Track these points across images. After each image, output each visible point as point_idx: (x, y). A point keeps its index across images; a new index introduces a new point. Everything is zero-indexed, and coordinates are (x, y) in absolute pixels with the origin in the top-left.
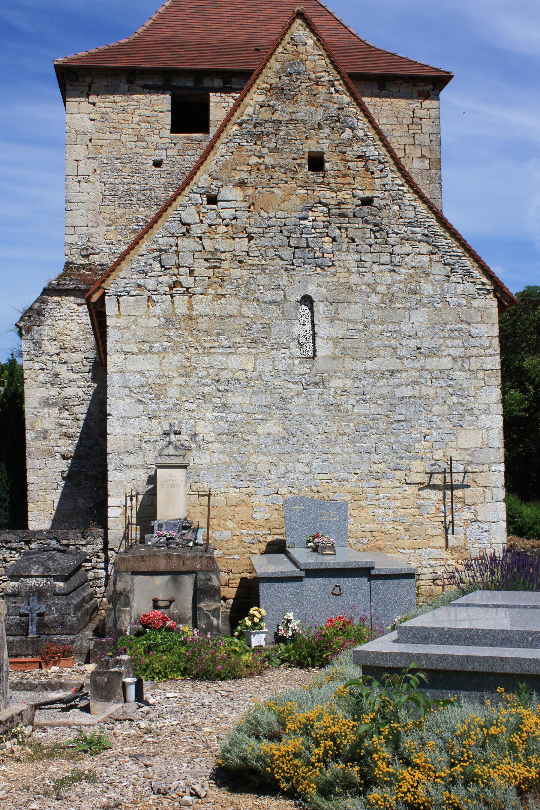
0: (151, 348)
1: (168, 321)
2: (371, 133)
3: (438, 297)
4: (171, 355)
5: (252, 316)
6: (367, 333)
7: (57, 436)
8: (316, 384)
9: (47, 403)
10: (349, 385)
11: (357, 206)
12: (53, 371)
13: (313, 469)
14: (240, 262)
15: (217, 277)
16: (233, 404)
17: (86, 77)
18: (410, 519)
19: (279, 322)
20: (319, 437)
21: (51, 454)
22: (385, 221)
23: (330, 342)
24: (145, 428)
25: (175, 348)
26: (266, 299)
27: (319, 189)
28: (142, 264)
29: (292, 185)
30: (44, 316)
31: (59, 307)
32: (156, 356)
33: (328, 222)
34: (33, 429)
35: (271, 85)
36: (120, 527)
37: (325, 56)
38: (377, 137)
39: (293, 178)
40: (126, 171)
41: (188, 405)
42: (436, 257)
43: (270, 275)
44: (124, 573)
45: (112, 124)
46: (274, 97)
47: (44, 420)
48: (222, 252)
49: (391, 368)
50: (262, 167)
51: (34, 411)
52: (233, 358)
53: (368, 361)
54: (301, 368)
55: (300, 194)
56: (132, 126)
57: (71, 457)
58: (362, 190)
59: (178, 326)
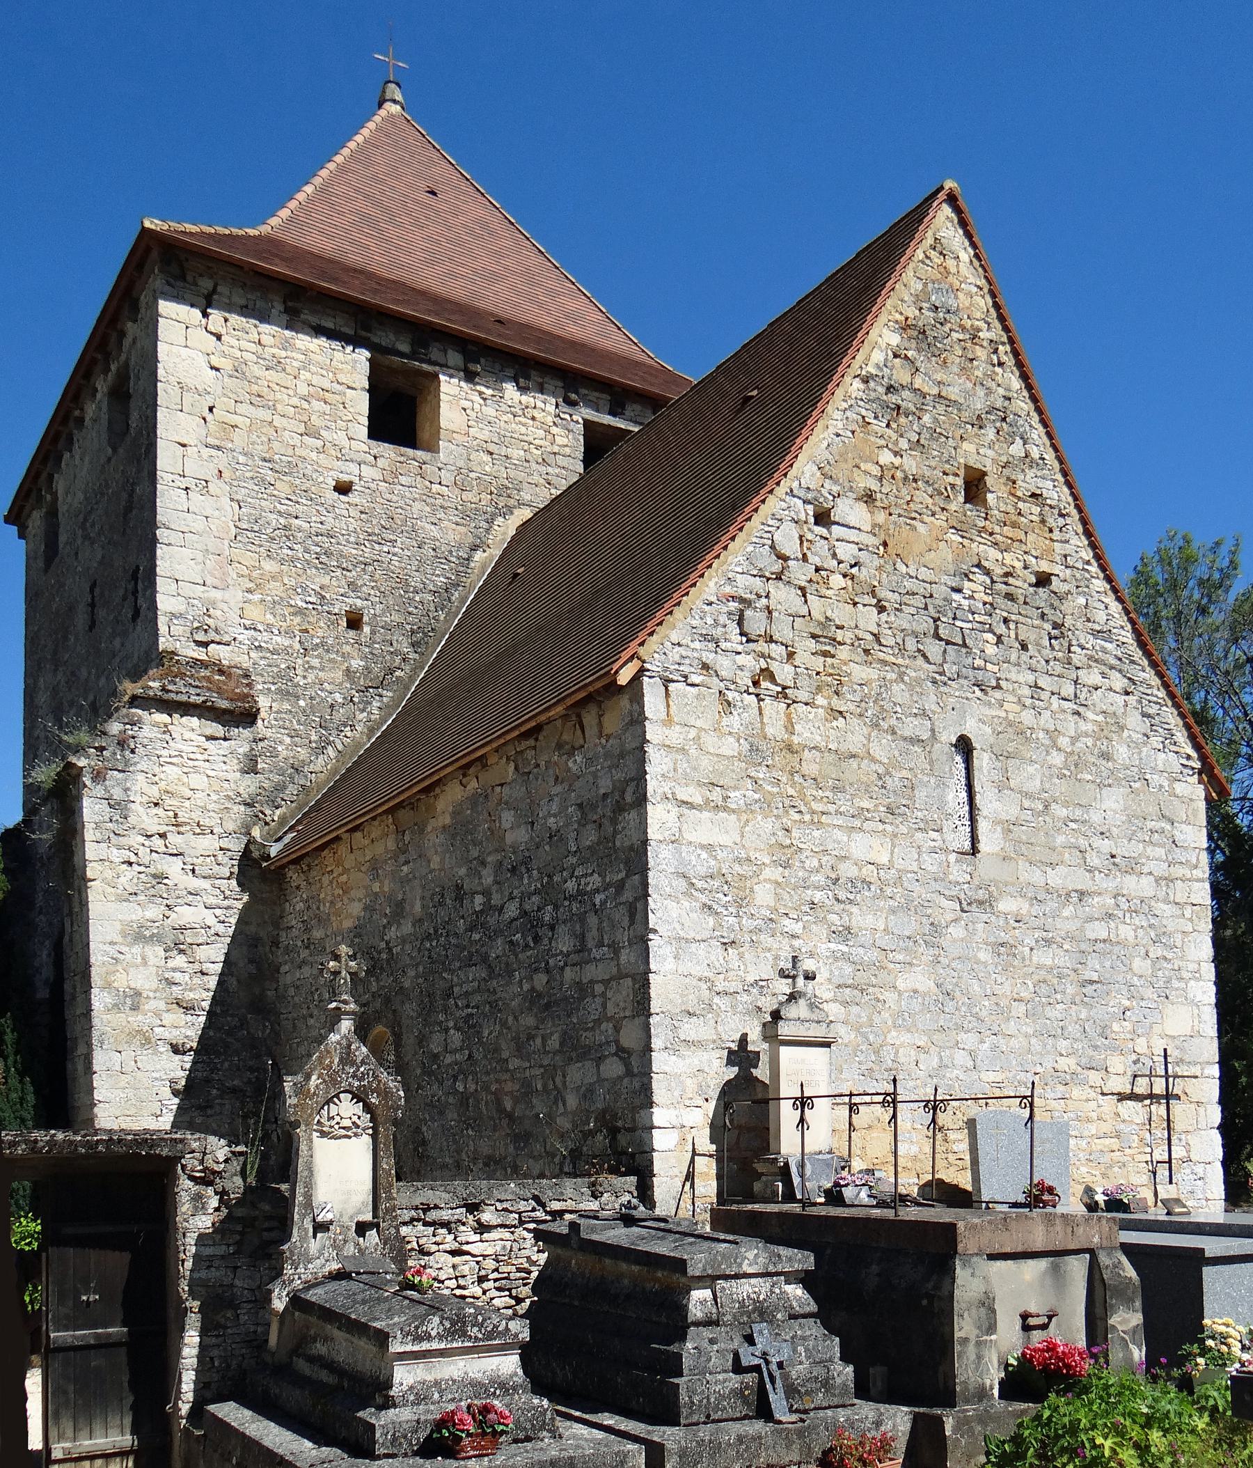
0: (726, 798)
1: (754, 749)
2: (1050, 456)
3: (1136, 769)
4: (760, 818)
5: (886, 761)
6: (1047, 819)
7: (162, 1005)
8: (981, 903)
9: (139, 936)
10: (1024, 912)
11: (1030, 585)
12: (152, 870)
13: (978, 1062)
14: (867, 652)
15: (831, 675)
16: (861, 929)
17: (201, 275)
18: (1106, 1159)
19: (926, 779)
20: (986, 1003)
21: (147, 1041)
22: (1069, 622)
23: (999, 829)
24: (718, 965)
25: (766, 804)
26: (907, 733)
27: (979, 539)
28: (710, 621)
29: (940, 521)
30: (133, 752)
31: (167, 737)
32: (733, 817)
33: (991, 604)
34: (108, 986)
35: (907, 319)
36: (676, 1171)
37: (986, 290)
38: (1056, 465)
39: (943, 509)
40: (283, 488)
41: (790, 926)
42: (1132, 699)
43: (911, 687)
44: (975, 1259)
45: (255, 388)
46: (914, 346)
47: (132, 971)
48: (838, 627)
49: (1079, 888)
50: (899, 474)
51: (112, 950)
52: (858, 836)
53: (1049, 870)
54: (958, 872)
55: (952, 541)
56: (295, 401)
57: (191, 1049)
58: (1037, 558)
59: (770, 762)
